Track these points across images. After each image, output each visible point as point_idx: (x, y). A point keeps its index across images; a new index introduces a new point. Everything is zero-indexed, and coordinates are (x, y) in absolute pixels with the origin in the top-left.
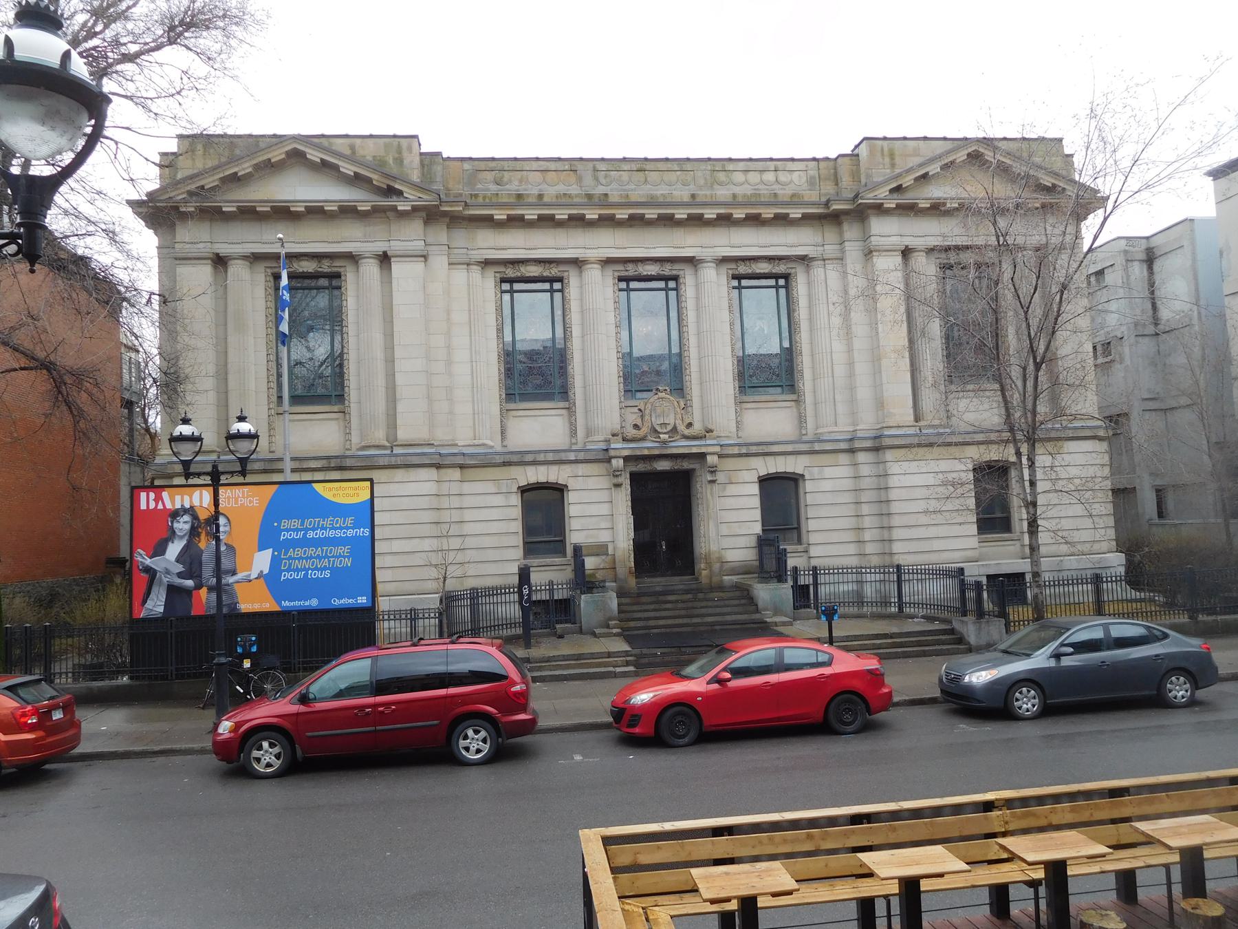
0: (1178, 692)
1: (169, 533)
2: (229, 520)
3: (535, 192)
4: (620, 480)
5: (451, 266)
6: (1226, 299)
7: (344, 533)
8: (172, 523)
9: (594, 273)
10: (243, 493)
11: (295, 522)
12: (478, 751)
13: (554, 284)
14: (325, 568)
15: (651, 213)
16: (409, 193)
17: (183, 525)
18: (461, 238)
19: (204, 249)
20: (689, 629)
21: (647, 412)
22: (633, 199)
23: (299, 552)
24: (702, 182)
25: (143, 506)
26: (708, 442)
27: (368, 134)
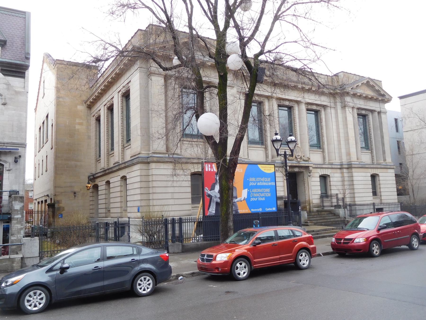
6: (404, 132)
11: (251, 179)
14: (263, 197)
25: (207, 170)
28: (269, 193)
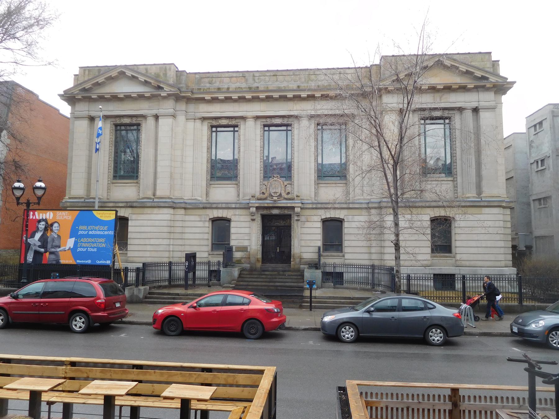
0: (436, 337)
1: (36, 229)
2: (59, 225)
3: (226, 86)
4: (254, 217)
5: (187, 120)
7: (104, 233)
8: (38, 224)
9: (250, 123)
10: (66, 214)
12: (80, 327)
13: (235, 128)
14: (95, 247)
15: (276, 95)
16: (166, 88)
17: (42, 226)
18: (192, 107)
19: (86, 113)
20: (266, 288)
21: (268, 186)
22: (270, 88)
23: (85, 240)
24: (303, 80)
26: (296, 201)
27: (153, 64)
28: (104, 243)
